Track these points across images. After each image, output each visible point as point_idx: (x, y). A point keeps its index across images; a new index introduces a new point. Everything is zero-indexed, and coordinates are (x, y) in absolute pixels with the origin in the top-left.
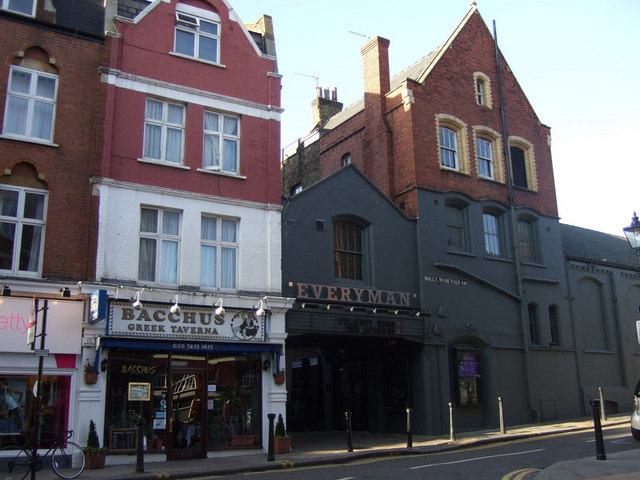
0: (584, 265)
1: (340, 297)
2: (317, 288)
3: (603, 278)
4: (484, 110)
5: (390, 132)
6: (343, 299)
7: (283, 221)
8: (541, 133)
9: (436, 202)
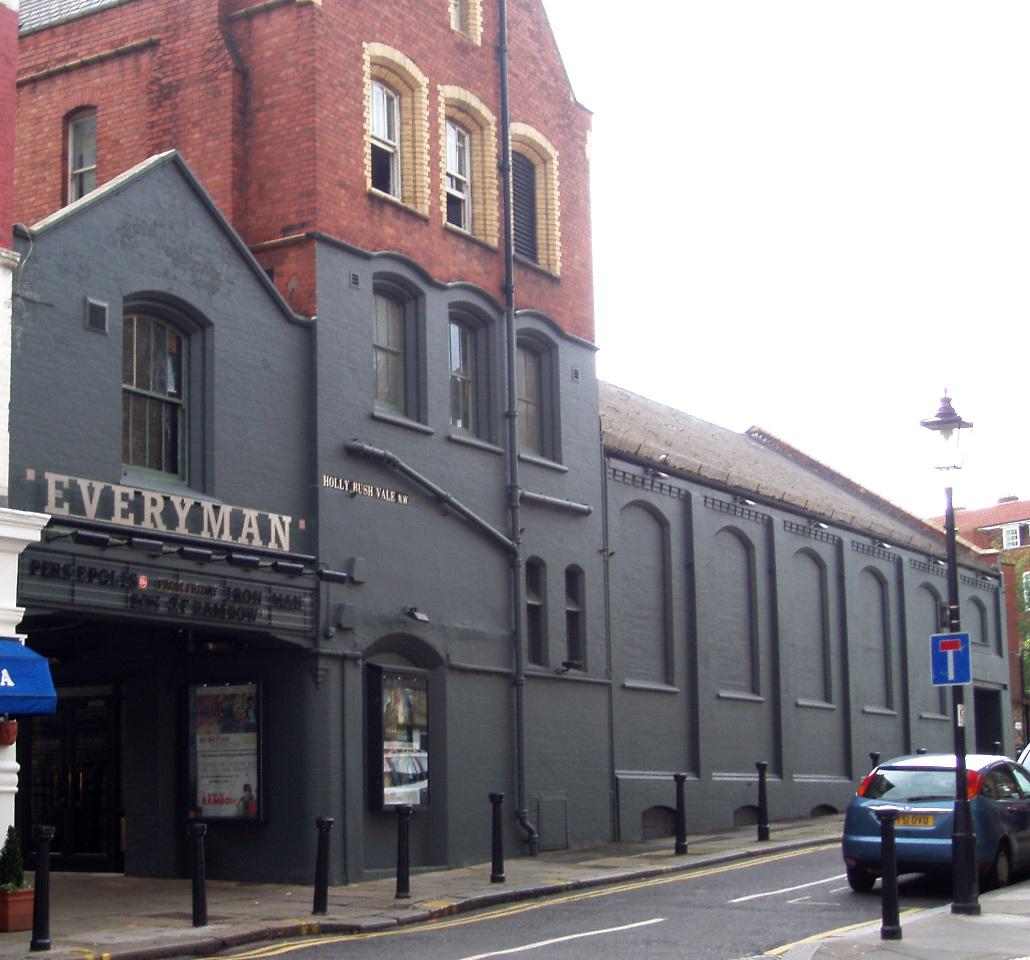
0: (636, 470)
1: (139, 519)
2: (91, 489)
3: (669, 508)
4: (464, 48)
5: (243, 75)
6: (147, 525)
7: (15, 296)
8: (570, 122)
9: (355, 280)
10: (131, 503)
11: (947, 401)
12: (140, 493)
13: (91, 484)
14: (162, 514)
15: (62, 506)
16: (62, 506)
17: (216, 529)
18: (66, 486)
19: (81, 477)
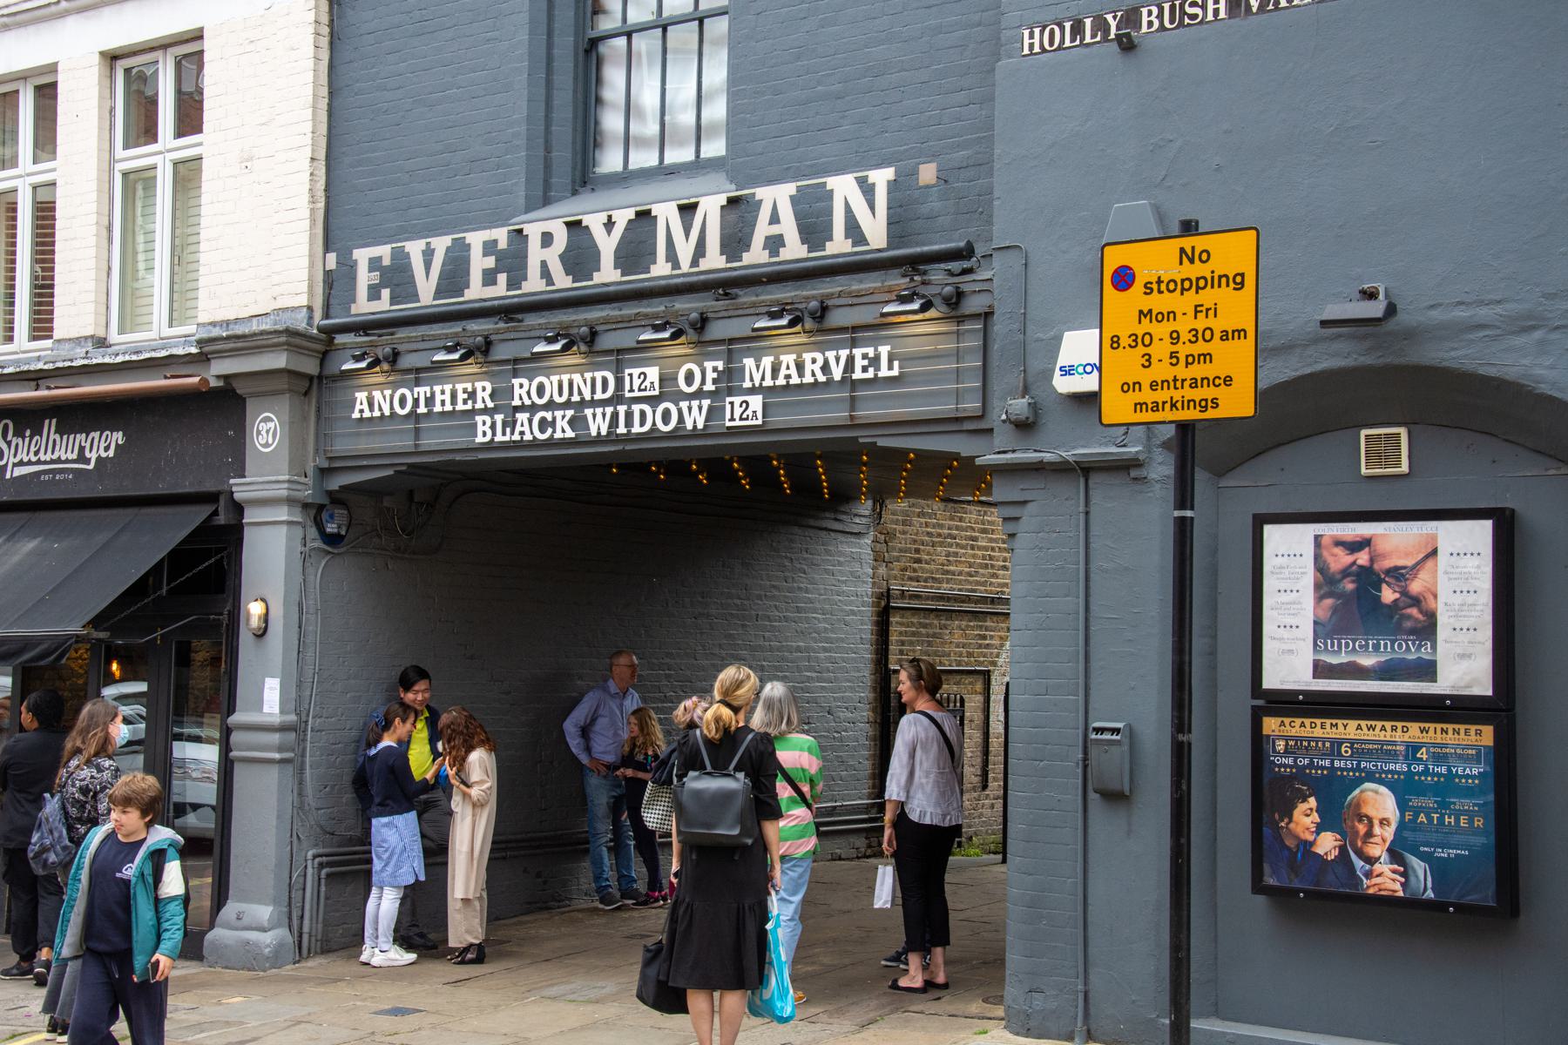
10: (501, 257)
11: (609, 235)
15: (494, 283)
16: (494, 283)
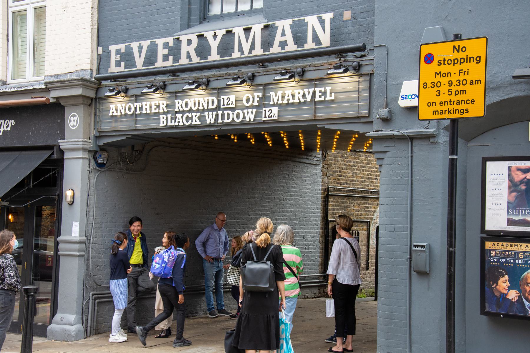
10: (170, 49)
12: (202, 35)
13: (140, 44)
14: (196, 50)
17: (246, 47)
18: (123, 51)
19: (131, 42)
